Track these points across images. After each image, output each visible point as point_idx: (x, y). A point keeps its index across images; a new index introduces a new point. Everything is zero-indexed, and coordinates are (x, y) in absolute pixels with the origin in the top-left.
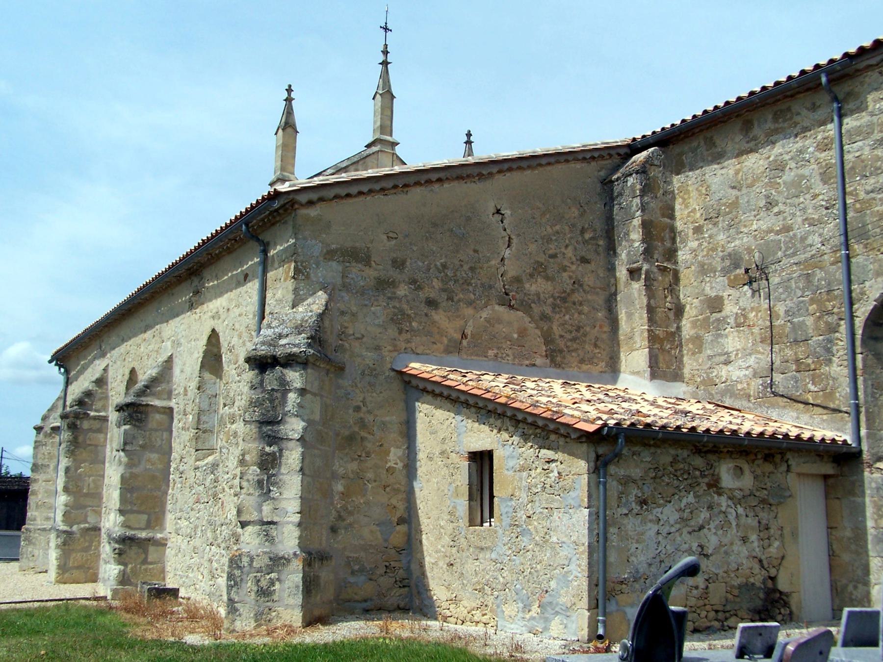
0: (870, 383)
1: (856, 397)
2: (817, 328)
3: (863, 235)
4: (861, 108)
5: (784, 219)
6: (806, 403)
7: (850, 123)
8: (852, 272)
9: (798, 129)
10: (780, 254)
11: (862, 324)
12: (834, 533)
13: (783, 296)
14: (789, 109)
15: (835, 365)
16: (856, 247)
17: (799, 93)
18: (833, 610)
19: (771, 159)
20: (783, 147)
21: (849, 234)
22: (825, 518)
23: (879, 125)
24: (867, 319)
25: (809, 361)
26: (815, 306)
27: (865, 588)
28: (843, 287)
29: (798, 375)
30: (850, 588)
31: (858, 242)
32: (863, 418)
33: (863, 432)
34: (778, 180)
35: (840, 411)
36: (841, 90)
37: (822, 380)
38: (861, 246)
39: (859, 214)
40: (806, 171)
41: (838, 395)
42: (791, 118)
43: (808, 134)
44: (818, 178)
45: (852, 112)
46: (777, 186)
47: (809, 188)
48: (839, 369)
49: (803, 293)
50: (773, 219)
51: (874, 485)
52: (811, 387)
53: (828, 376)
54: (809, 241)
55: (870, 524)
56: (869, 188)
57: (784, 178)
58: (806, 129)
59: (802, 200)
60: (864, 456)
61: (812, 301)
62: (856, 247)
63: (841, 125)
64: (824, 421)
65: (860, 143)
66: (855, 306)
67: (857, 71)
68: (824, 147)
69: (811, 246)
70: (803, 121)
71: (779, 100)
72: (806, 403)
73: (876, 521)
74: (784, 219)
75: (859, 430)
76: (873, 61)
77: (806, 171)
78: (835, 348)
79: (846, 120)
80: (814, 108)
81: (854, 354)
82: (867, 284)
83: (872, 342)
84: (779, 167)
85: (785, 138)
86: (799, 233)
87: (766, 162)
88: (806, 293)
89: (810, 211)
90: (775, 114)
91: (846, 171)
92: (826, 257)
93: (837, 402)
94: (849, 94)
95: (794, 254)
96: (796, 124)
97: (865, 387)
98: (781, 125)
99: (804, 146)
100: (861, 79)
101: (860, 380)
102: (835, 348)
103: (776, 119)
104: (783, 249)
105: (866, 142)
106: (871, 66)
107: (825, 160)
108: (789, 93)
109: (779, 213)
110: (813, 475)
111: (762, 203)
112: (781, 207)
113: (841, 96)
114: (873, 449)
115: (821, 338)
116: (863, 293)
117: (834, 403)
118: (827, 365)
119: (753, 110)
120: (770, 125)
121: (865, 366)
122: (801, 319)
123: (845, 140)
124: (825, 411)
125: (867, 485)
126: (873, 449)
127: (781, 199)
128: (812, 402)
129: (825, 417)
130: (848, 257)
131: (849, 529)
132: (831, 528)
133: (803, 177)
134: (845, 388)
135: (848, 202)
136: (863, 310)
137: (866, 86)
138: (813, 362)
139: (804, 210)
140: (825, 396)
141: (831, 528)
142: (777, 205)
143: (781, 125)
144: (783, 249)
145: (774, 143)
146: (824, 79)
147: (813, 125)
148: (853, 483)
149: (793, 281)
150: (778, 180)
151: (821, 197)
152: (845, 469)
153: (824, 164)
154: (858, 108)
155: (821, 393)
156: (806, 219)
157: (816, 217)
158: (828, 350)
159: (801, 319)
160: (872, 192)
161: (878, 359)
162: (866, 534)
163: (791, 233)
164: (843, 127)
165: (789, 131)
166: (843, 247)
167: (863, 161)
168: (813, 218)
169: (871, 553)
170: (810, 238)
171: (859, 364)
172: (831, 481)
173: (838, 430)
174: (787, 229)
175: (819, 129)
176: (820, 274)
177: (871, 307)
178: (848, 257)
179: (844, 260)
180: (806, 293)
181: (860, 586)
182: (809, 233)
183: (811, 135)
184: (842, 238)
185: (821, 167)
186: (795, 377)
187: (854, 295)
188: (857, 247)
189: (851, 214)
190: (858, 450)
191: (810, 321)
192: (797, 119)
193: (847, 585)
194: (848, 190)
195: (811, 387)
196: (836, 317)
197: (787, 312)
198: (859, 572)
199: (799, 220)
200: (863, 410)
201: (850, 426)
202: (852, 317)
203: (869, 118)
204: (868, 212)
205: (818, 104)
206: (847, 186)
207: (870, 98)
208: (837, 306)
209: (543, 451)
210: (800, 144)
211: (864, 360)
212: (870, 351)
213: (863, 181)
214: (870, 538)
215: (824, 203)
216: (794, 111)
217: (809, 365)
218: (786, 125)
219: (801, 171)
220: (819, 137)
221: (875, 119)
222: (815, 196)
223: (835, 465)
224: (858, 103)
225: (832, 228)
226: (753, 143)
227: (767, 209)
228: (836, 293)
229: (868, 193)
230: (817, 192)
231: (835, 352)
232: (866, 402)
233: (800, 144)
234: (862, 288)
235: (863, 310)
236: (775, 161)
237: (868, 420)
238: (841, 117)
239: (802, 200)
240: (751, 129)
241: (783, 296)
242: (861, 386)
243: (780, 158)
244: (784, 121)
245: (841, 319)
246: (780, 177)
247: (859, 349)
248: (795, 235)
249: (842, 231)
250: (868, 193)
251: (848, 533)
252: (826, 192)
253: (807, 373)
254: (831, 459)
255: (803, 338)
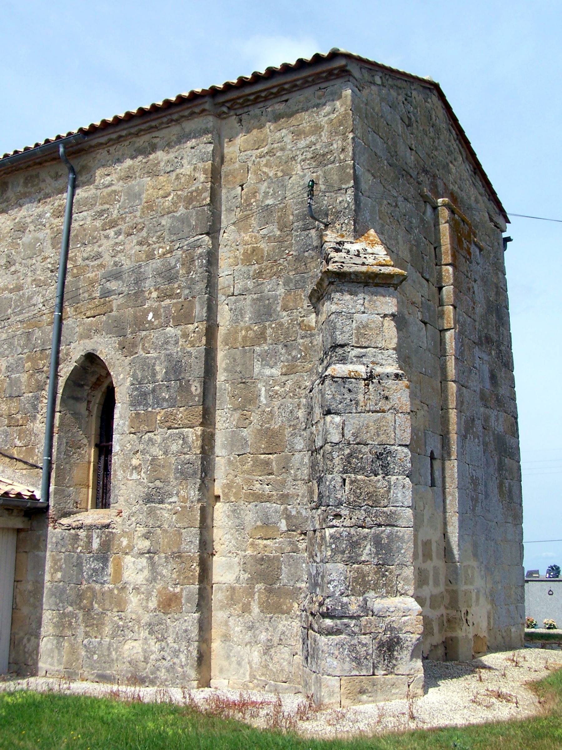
0: (65, 440)
1: (50, 454)
2: (29, 385)
3: (76, 299)
4: (90, 182)
5: (18, 278)
6: (12, 458)
7: (81, 193)
8: (63, 333)
9: (41, 195)
10: (10, 311)
11: (63, 384)
12: (19, 586)
13: (7, 352)
14: (37, 176)
15: (38, 422)
16: (68, 309)
17: (46, 161)
18: (9, 663)
19: (16, 221)
20: (28, 211)
21: (65, 295)
22: (13, 572)
23: (100, 198)
24: (68, 379)
25: (19, 416)
26: (29, 363)
27: (37, 640)
28: (53, 346)
29: (8, 429)
30: (25, 640)
31: (71, 305)
32: (53, 474)
33: (52, 488)
34: (19, 241)
35: (37, 467)
36: (77, 163)
37: (27, 436)
38: (73, 309)
39: (75, 279)
40: (41, 235)
41: (37, 450)
42: (38, 184)
43: (48, 200)
44: (49, 242)
45: (84, 184)
46: (17, 247)
47: (41, 251)
48: (39, 426)
49: (23, 350)
50: (9, 278)
51: (54, 540)
52: (18, 443)
53: (31, 432)
54: (34, 301)
55: (47, 577)
56: (85, 255)
57: (24, 239)
58: (48, 196)
59: (34, 261)
60: (50, 511)
61: (29, 358)
62: (68, 309)
63: (73, 195)
64: (23, 475)
65: (85, 213)
66: (61, 366)
67: (91, 147)
68: (57, 214)
69: (34, 305)
70: (46, 187)
71: (29, 166)
72: (12, 458)
73: (52, 574)
74: (18, 278)
75: (49, 486)
76: (103, 140)
77: (41, 235)
78: (40, 405)
79: (78, 191)
80: (57, 177)
81: (53, 411)
82: (73, 345)
83: (71, 402)
84: (21, 229)
85: (30, 202)
86: (27, 292)
87: (12, 223)
88: (25, 351)
89: (38, 273)
90: (26, 179)
91: (71, 237)
92: (44, 317)
93: (35, 458)
94: (84, 168)
95: (21, 312)
96: (41, 190)
97: (59, 445)
98: (29, 190)
99: (43, 211)
100: (93, 155)
101: (56, 436)
102: (40, 405)
103: (26, 184)
104: (13, 307)
105: (89, 212)
106: (101, 144)
107: (57, 226)
108: (37, 161)
109: (15, 272)
110: (8, 529)
111: (3, 262)
112: (17, 266)
113: (77, 169)
114: (59, 504)
115: (31, 395)
116: (68, 354)
117: (33, 459)
118: (32, 422)
119: (9, 173)
120: (20, 189)
121: (61, 424)
122: (17, 375)
123: (74, 210)
124: (25, 466)
125: (49, 540)
126: (59, 504)
127: (18, 259)
128: (16, 456)
129: (24, 472)
130: (61, 319)
131: (31, 583)
132: (18, 581)
133: (37, 240)
134: (42, 446)
135: (68, 266)
136: (65, 370)
137: (96, 162)
138: (22, 418)
139: (34, 271)
140: (26, 451)
141: (18, 581)
142: (14, 264)
143: (29, 190)
144: (13, 307)
145: (21, 206)
146: (61, 150)
147: (53, 193)
148: (39, 538)
149: (16, 338)
150: (19, 241)
151: (49, 260)
152: (35, 523)
153: (55, 229)
154: (88, 181)
155: (24, 448)
156: (34, 280)
157: (42, 278)
158: (35, 407)
159: (17, 375)
160: (87, 259)
161: (76, 419)
162: (43, 587)
163: (21, 292)
164: (75, 197)
165: (34, 196)
166: (57, 309)
167: (84, 230)
168: (40, 279)
169: (45, 607)
170: (35, 298)
171: (57, 422)
172: (22, 535)
173: (33, 485)
174: (19, 288)
175: (57, 197)
176: (38, 333)
177: (72, 368)
178: (61, 319)
179: (56, 322)
180: (25, 351)
181: (33, 638)
182: (34, 293)
183: (50, 202)
184: (57, 300)
185: (53, 233)
186: (7, 432)
187: (61, 355)
188: (69, 310)
189: (69, 279)
190: (45, 505)
191: (24, 377)
192: (42, 185)
193: (23, 638)
194: (70, 255)
195: (18, 443)
196: (44, 375)
197: (8, 367)
198: (34, 626)
199: (29, 280)
200: (54, 466)
201: (41, 483)
202: (56, 376)
203: (94, 191)
204: (82, 277)
205: (60, 174)
206: (70, 252)
207: (98, 173)
208: (46, 364)
209: (456, 490)
210: (41, 209)
211: (61, 419)
212: (69, 410)
213: (82, 249)
214: (45, 591)
215: (50, 266)
216: (41, 178)
217: (18, 420)
218: (33, 190)
219: (37, 235)
220: (56, 204)
221: (99, 192)
222: (45, 258)
223: (26, 519)
224: (89, 176)
225: (53, 290)
226: (6, 204)
227: (7, 268)
228: (47, 352)
229: (84, 259)
230: (47, 255)
231: (39, 409)
232: (58, 458)
233: (41, 209)
234: (68, 349)
235: (65, 370)
236: (19, 222)
237: (57, 476)
238: (74, 187)
239: (34, 261)
240: (6, 191)
241: (7, 352)
242: (55, 443)
243: (24, 220)
244: (33, 186)
245: (48, 378)
246: (21, 238)
247: (58, 408)
248: (23, 294)
249: (59, 294)
250: (84, 259)
251: (30, 587)
252: (53, 255)
253: (15, 428)
254: (22, 513)
255: (17, 394)
